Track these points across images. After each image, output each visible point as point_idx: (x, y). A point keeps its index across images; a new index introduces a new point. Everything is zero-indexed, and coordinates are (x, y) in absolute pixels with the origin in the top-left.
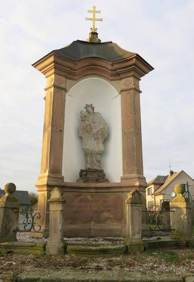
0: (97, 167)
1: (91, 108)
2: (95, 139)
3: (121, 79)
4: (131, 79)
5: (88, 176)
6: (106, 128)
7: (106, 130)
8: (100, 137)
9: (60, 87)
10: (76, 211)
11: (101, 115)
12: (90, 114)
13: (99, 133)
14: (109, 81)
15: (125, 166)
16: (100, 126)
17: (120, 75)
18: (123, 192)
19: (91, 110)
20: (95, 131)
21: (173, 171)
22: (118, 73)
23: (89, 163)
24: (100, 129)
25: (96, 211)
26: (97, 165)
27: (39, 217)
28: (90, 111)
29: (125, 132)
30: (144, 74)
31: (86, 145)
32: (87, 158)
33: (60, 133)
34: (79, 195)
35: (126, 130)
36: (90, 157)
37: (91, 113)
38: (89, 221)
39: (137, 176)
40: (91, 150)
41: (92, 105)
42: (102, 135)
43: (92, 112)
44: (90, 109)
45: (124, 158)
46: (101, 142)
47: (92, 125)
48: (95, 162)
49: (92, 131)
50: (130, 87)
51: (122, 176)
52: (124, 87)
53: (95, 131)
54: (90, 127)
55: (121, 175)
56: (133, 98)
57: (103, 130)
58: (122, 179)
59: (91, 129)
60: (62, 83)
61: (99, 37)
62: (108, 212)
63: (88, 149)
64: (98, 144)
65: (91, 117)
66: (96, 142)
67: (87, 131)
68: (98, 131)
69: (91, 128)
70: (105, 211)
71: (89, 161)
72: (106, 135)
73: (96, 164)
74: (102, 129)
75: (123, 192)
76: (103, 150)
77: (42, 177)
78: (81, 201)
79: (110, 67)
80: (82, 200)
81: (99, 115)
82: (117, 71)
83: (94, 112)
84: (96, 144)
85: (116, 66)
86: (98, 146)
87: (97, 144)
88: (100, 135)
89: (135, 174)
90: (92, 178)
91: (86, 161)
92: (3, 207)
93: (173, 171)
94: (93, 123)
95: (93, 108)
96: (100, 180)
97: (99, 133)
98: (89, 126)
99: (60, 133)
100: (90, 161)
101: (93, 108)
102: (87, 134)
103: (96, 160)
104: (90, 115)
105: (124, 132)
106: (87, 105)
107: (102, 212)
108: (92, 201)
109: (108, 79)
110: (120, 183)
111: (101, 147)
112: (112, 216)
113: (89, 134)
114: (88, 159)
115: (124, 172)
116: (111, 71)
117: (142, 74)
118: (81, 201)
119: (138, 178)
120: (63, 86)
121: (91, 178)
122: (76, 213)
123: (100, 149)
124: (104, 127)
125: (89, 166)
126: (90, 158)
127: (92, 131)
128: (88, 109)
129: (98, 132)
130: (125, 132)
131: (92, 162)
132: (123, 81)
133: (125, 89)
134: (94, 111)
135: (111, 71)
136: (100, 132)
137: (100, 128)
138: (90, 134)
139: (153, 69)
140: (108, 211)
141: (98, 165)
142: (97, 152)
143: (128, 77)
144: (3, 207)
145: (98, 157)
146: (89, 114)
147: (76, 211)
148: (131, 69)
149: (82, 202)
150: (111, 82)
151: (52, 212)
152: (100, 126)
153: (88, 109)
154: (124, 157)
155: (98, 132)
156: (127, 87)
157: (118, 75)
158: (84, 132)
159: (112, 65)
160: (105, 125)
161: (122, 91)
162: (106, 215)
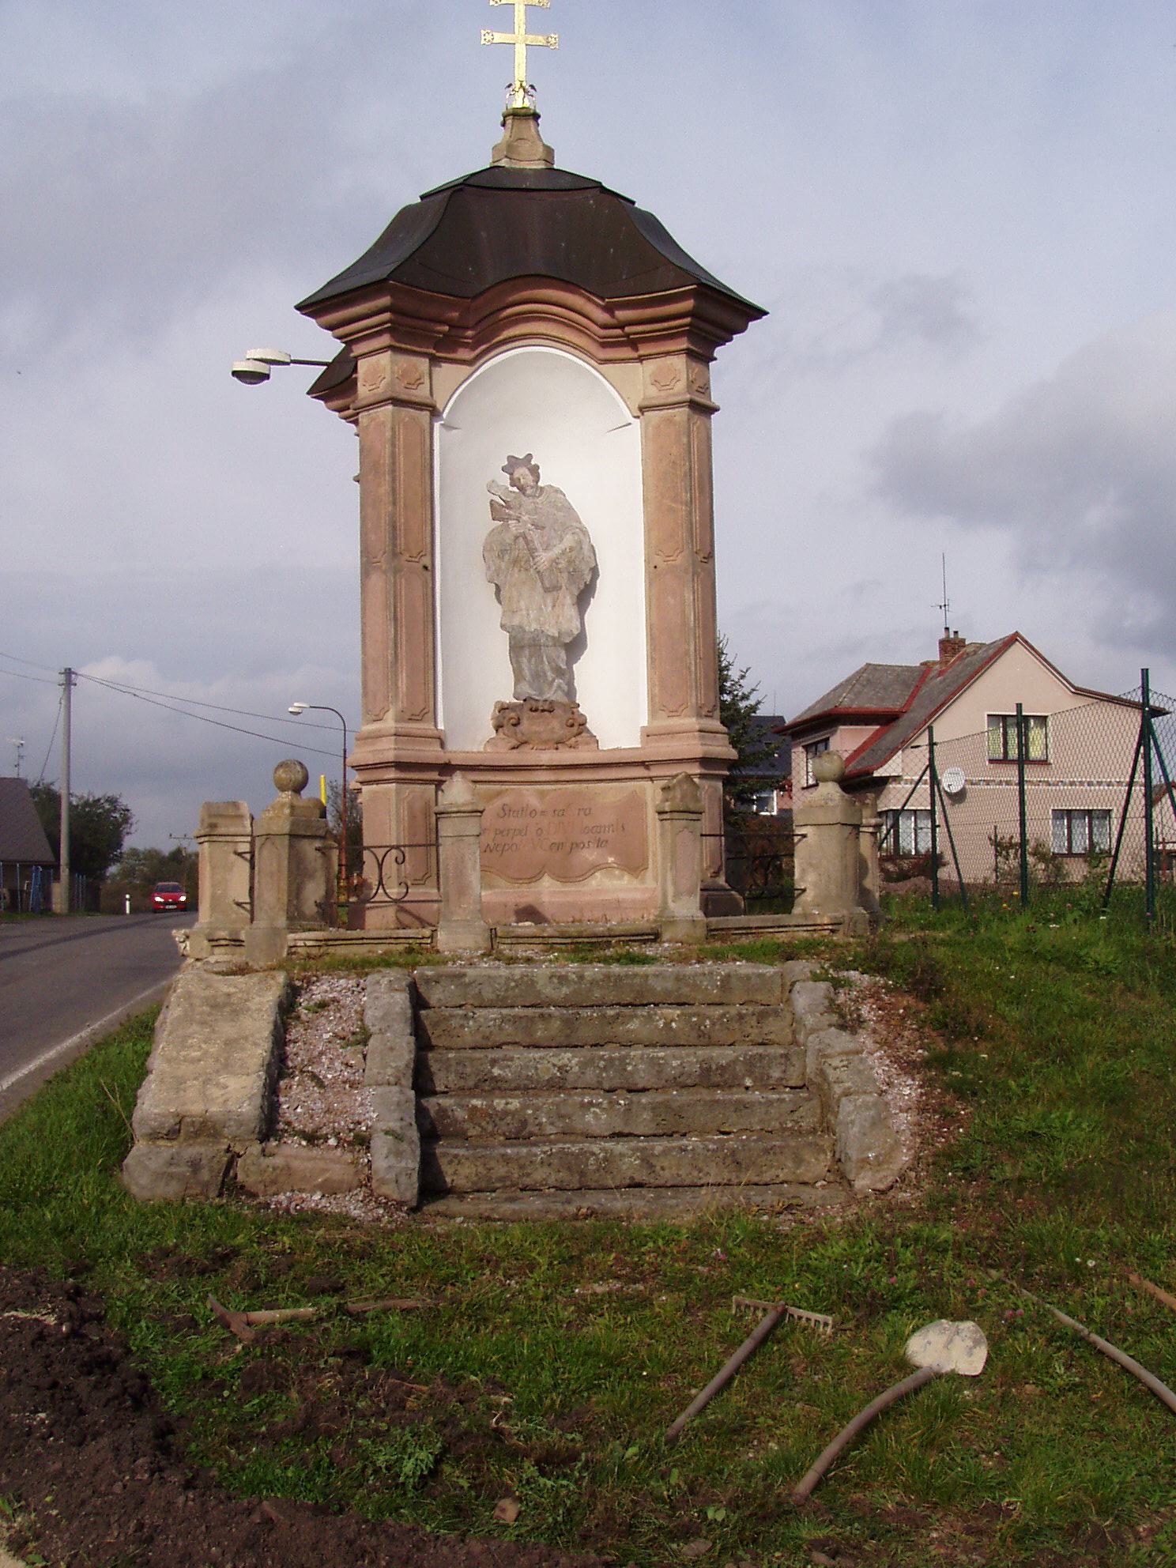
0: (556, 691)
1: (529, 469)
2: (547, 590)
3: (641, 359)
4: (679, 363)
6: (586, 547)
7: (586, 553)
8: (563, 579)
9: (414, 399)
12: (524, 494)
13: (560, 566)
14: (595, 364)
15: (657, 691)
16: (565, 540)
18: (832, 924)
20: (544, 558)
23: (528, 678)
24: (564, 552)
25: (559, 846)
26: (555, 684)
27: (400, 861)
30: (723, 334)
32: (518, 662)
34: (499, 794)
35: (658, 560)
36: (531, 656)
37: (529, 492)
38: (535, 878)
39: (697, 727)
41: (530, 456)
42: (569, 573)
44: (521, 472)
46: (569, 600)
47: (535, 536)
49: (533, 559)
51: (646, 724)
52: (654, 394)
53: (544, 558)
54: (527, 544)
56: (685, 440)
57: (574, 554)
58: (648, 735)
59: (532, 551)
63: (521, 627)
64: (557, 609)
66: (549, 602)
67: (515, 562)
71: (527, 672)
73: (554, 680)
74: (571, 549)
75: (832, 924)
77: (372, 738)
79: (602, 316)
80: (506, 808)
81: (559, 495)
82: (627, 329)
83: (540, 484)
84: (550, 609)
85: (622, 315)
86: (558, 616)
88: (565, 575)
90: (540, 733)
91: (519, 676)
93: (960, 636)
94: (537, 527)
95: (535, 471)
97: (560, 566)
98: (521, 539)
100: (530, 670)
101: (537, 467)
102: (516, 570)
103: (552, 669)
104: (524, 498)
105: (652, 566)
107: (576, 846)
109: (592, 356)
110: (637, 748)
111: (565, 619)
114: (523, 666)
115: (653, 713)
116: (605, 327)
117: (713, 323)
119: (700, 731)
120: (421, 393)
123: (565, 627)
124: (580, 542)
125: (527, 690)
126: (529, 661)
127: (533, 559)
128: (516, 475)
129: (557, 564)
131: (538, 676)
132: (650, 366)
134: (537, 478)
135: (605, 327)
137: (562, 546)
139: (758, 313)
141: (559, 687)
142: (553, 638)
143: (668, 353)
145: (558, 657)
148: (676, 327)
150: (605, 368)
151: (449, 841)
152: (561, 540)
155: (557, 564)
156: (663, 393)
157: (633, 343)
159: (609, 309)
160: (582, 536)
161: (642, 409)
162: (590, 855)
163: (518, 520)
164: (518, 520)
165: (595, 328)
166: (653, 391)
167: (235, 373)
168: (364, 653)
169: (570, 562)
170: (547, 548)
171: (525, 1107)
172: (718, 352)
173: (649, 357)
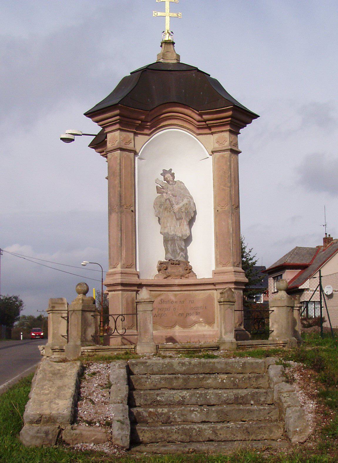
1: (171, 174)
2: (177, 219)
3: (212, 133)
5: (169, 269)
6: (192, 203)
8: (184, 215)
10: (156, 314)
11: (184, 184)
13: (182, 210)
14: (195, 135)
15: (218, 257)
17: (212, 128)
18: (283, 344)
19: (171, 178)
20: (176, 207)
21: (331, 236)
22: (209, 125)
24: (184, 205)
25: (182, 314)
28: (168, 179)
29: (218, 211)
31: (165, 227)
33: (131, 214)
34: (159, 295)
35: (219, 208)
37: (171, 183)
38: (173, 326)
39: (233, 270)
40: (172, 235)
41: (171, 170)
42: (186, 213)
43: (172, 181)
44: (168, 175)
45: (216, 246)
46: (185, 223)
47: (173, 199)
48: (178, 251)
49: (172, 208)
50: (225, 147)
51: (214, 269)
52: (217, 146)
53: (176, 207)
54: (170, 202)
55: (213, 268)
56: (229, 164)
57: (187, 206)
58: (215, 273)
59: (172, 205)
60: (130, 142)
61: (178, 49)
62: (196, 315)
63: (168, 233)
65: (170, 187)
66: (178, 224)
67: (166, 209)
68: (180, 209)
69: (171, 204)
70: (192, 314)
71: (170, 250)
72: (192, 213)
73: (180, 253)
74: (186, 204)
75: (283, 344)
76: (188, 235)
78: (162, 303)
79: (198, 118)
81: (182, 184)
82: (207, 122)
83: (175, 180)
85: (205, 117)
87: (180, 225)
88: (184, 214)
89: (230, 266)
91: (167, 251)
92: (80, 310)
93: (331, 236)
94: (174, 196)
95: (173, 175)
96: (186, 275)
98: (168, 200)
99: (131, 214)
100: (171, 249)
101: (174, 174)
103: (179, 249)
104: (169, 185)
105: (216, 210)
106: (164, 170)
107: (188, 314)
108: (176, 302)
109: (194, 132)
111: (184, 230)
112: (202, 319)
113: (169, 213)
114: (169, 248)
115: (217, 265)
116: (199, 121)
118: (162, 303)
119: (234, 272)
120: (131, 146)
121: (173, 272)
122: (157, 316)
123: (184, 233)
124: (190, 202)
125: (170, 256)
126: (171, 246)
127: (172, 208)
128: (166, 177)
130: (218, 211)
131: (174, 251)
132: (216, 136)
133: (218, 150)
134: (174, 178)
135: (199, 121)
136: (183, 210)
138: (170, 212)
140: (197, 314)
141: (182, 255)
142: (180, 237)
143: (222, 131)
144: (80, 309)
145: (182, 244)
146: (168, 184)
147: (156, 314)
149: (163, 303)
150: (199, 137)
151: (141, 313)
152: (183, 201)
153: (166, 177)
154: (216, 245)
156: (220, 146)
157: (209, 128)
158: (161, 210)
159: (200, 115)
160: (190, 199)
161: (213, 152)
162: (193, 318)
163: (167, 193)
164: (167, 193)
165: (195, 122)
166: (217, 145)
167: (61, 139)
168: (109, 243)
169: (186, 209)
170: (177, 204)
171: (169, 411)
172: (241, 131)
173: (215, 133)
